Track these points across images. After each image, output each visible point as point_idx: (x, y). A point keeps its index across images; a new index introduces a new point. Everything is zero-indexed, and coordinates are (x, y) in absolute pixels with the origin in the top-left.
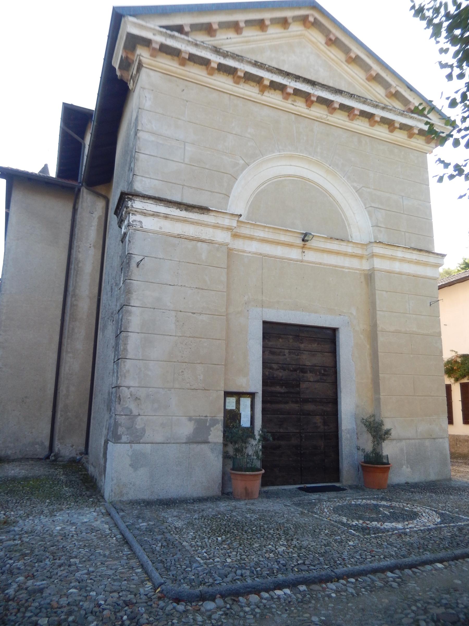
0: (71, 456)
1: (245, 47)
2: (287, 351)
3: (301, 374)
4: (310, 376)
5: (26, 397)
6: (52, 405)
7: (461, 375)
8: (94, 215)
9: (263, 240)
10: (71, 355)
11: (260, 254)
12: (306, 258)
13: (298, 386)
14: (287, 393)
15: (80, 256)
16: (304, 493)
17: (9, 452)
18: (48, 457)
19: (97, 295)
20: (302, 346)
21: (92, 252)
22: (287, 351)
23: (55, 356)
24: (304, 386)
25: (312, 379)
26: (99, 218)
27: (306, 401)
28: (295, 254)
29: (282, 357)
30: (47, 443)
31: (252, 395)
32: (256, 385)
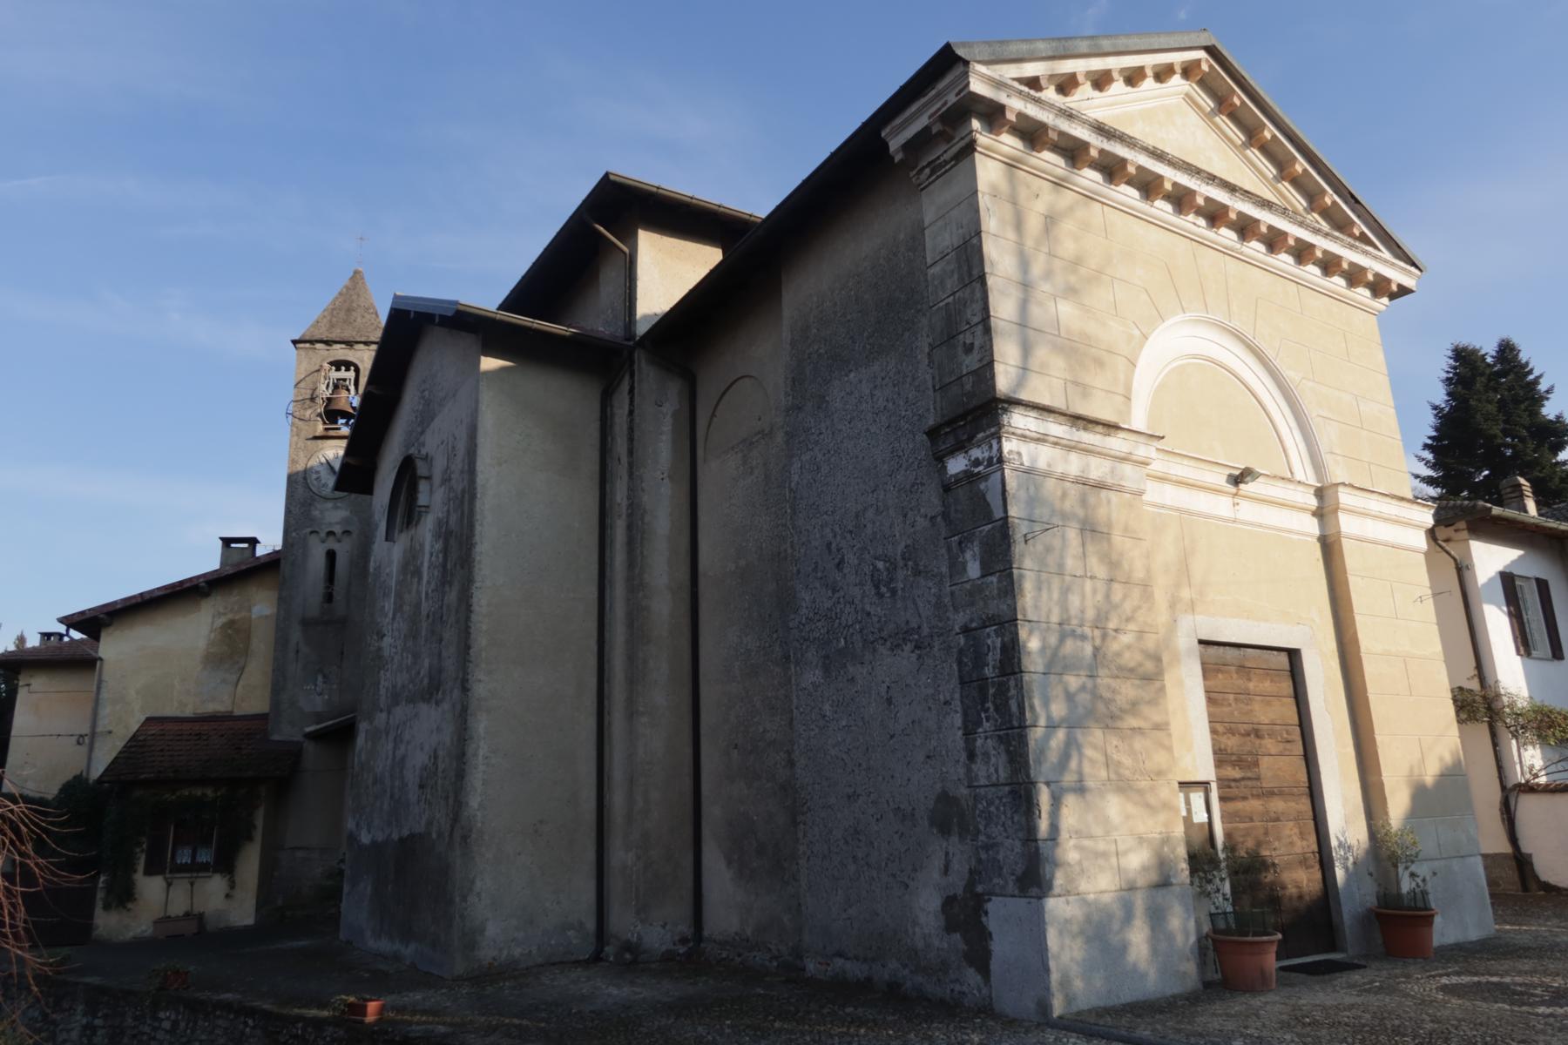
0: (664, 948)
1: (1118, 110)
2: (1231, 697)
3: (1258, 741)
4: (1269, 744)
5: (541, 822)
6: (593, 835)
7: (440, 671)
8: (664, 409)
9: (1181, 483)
10: (644, 719)
11: (1177, 510)
12: (1241, 516)
13: (1256, 764)
14: (1243, 779)
15: (645, 498)
16: (1302, 976)
17: (517, 952)
18: (597, 958)
19: (688, 583)
20: (1251, 685)
21: (666, 489)
22: (1231, 697)
23: (591, 723)
24: (1265, 762)
25: (1273, 751)
26: (675, 415)
27: (1271, 794)
28: (1221, 506)
29: (1226, 709)
30: (591, 925)
31: (1205, 785)
32: (1205, 769)
